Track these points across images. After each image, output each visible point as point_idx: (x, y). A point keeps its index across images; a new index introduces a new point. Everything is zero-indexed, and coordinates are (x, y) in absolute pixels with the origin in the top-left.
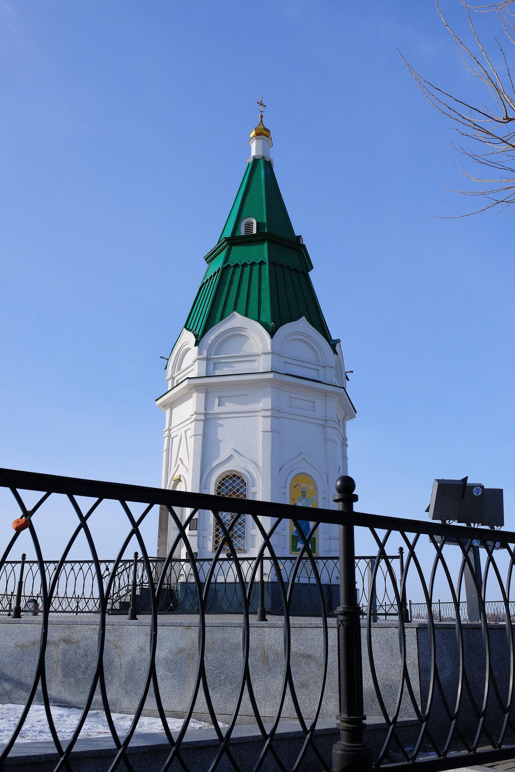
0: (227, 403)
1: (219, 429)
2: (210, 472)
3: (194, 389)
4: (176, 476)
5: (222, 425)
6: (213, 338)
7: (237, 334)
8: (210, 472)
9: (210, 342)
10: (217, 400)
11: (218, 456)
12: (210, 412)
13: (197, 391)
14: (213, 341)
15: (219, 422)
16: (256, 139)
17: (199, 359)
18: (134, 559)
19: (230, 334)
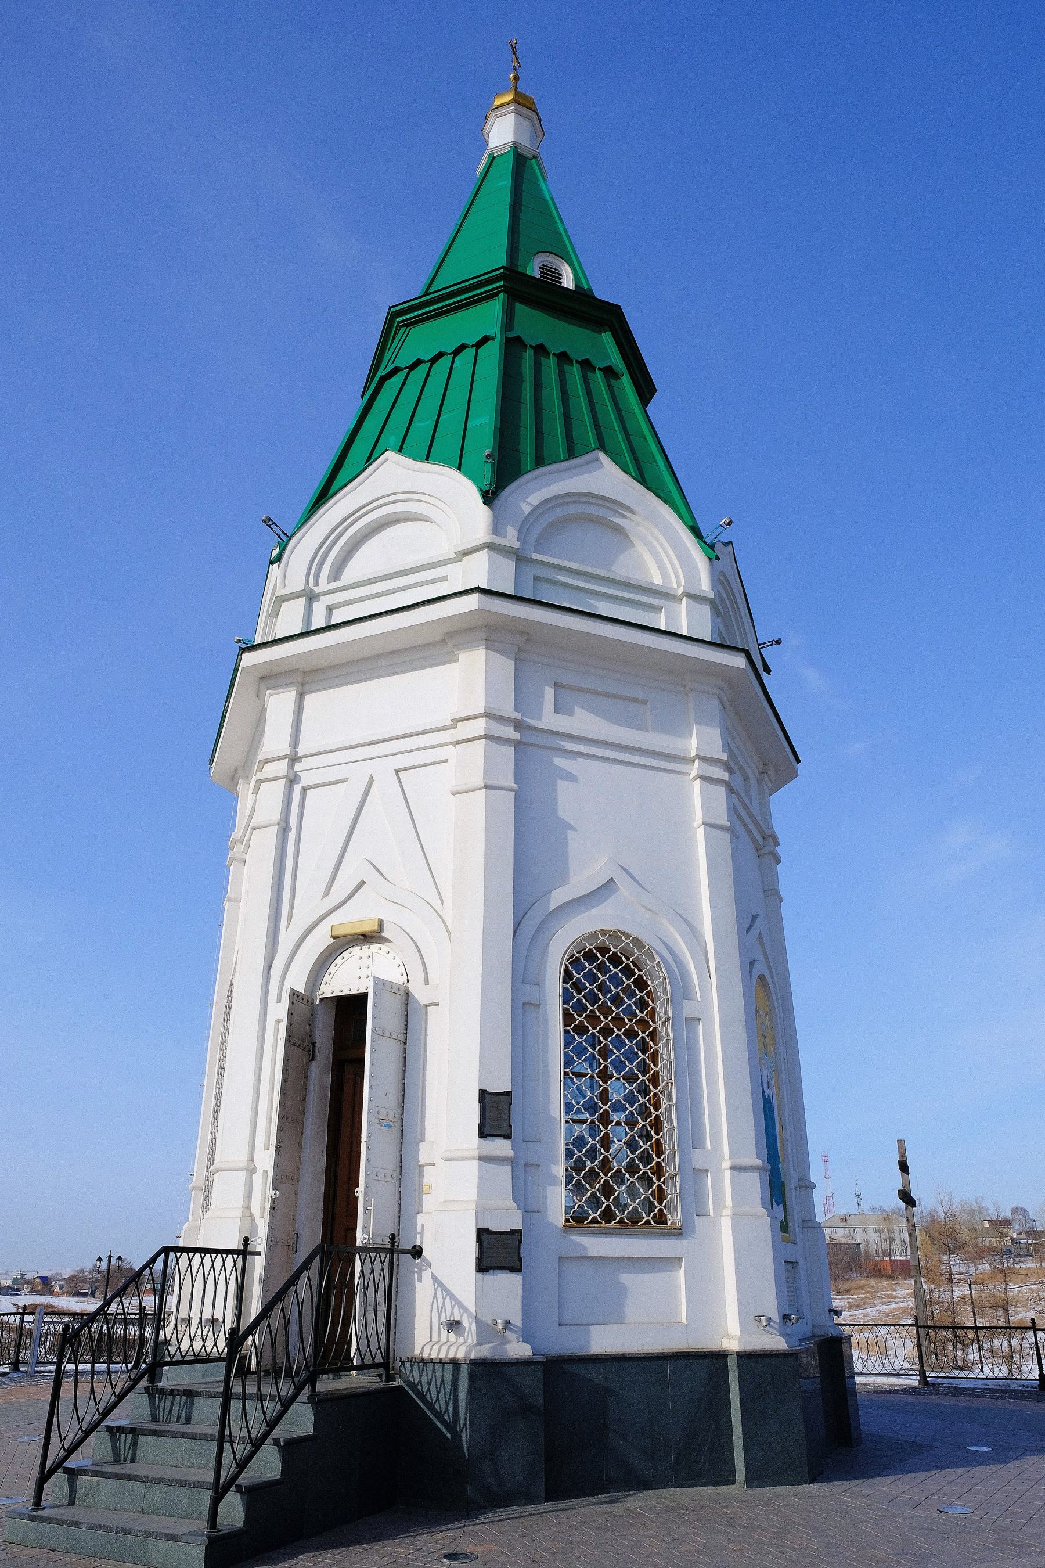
0: (578, 710)
1: (562, 785)
2: (539, 929)
3: (483, 634)
4: (356, 916)
5: (572, 778)
6: (535, 499)
7: (600, 517)
8: (539, 929)
9: (527, 509)
10: (549, 693)
11: (562, 876)
12: (532, 722)
13: (490, 644)
14: (536, 508)
15: (558, 761)
16: (516, 112)
17: (491, 547)
18: (242, 1248)
19: (581, 509)
